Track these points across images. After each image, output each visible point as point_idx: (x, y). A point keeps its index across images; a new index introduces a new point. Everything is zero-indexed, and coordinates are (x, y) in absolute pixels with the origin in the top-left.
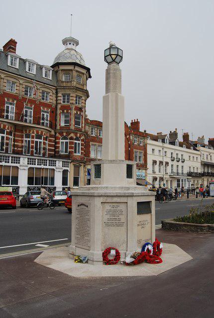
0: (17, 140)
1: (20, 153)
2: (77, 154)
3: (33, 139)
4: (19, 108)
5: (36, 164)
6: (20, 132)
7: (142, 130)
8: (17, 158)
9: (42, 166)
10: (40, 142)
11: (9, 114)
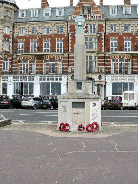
0: (134, 64)
5: (55, 80)
6: (135, 59)
9: (50, 81)
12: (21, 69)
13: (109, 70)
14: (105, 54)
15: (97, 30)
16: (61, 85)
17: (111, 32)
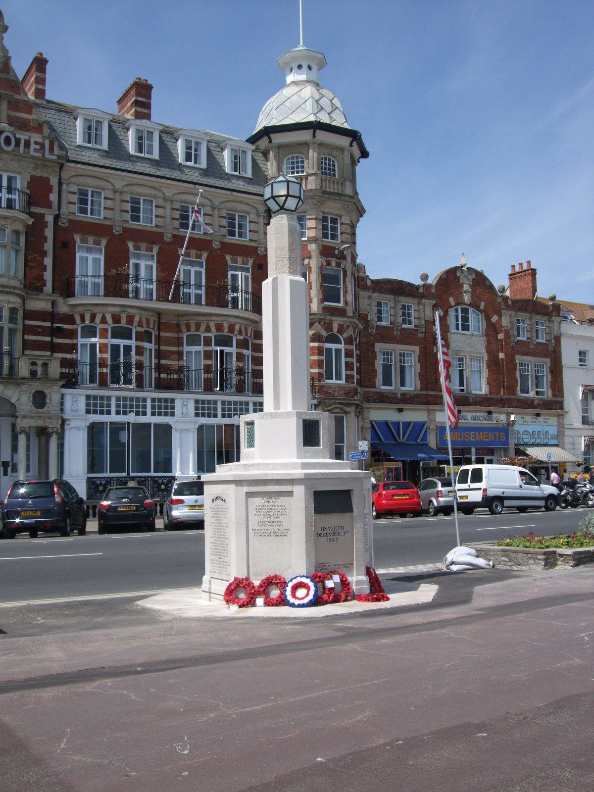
1: (178, 386)
2: (334, 381)
3: (104, 341)
4: (167, 264)
6: (171, 331)
7: (543, 292)
8: (166, 400)
9: (131, 418)
10: (128, 349)
11: (142, 286)
12: (208, 369)
13: (67, 370)
14: (54, 303)
15: (25, 198)
16: (173, 431)
17: (80, 217)
